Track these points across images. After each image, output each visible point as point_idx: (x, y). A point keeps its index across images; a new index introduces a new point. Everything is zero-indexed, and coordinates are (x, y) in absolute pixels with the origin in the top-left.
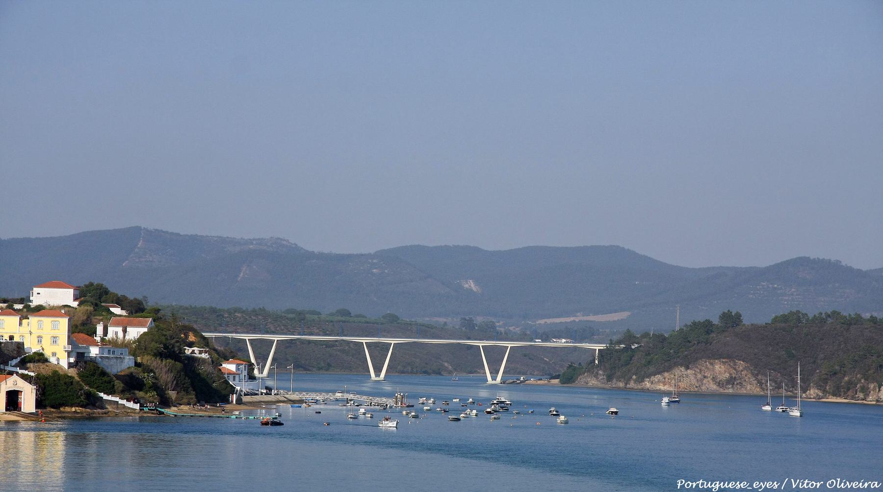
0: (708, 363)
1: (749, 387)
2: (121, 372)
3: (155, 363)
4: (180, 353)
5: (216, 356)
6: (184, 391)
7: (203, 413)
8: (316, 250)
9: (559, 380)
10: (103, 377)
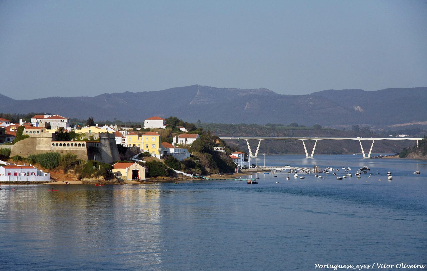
2: (184, 159)
3: (200, 155)
4: (212, 150)
5: (229, 150)
6: (213, 167)
7: (222, 178)
8: (282, 94)
9: (399, 156)
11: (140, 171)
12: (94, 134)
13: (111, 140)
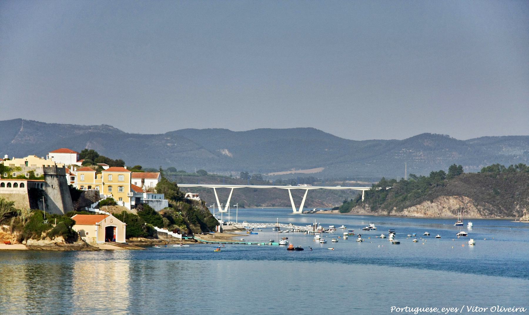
0: (445, 199)
1: (472, 214)
9: (338, 210)
10: (155, 215)
11: (117, 229)
12: (35, 167)
13: (61, 178)
